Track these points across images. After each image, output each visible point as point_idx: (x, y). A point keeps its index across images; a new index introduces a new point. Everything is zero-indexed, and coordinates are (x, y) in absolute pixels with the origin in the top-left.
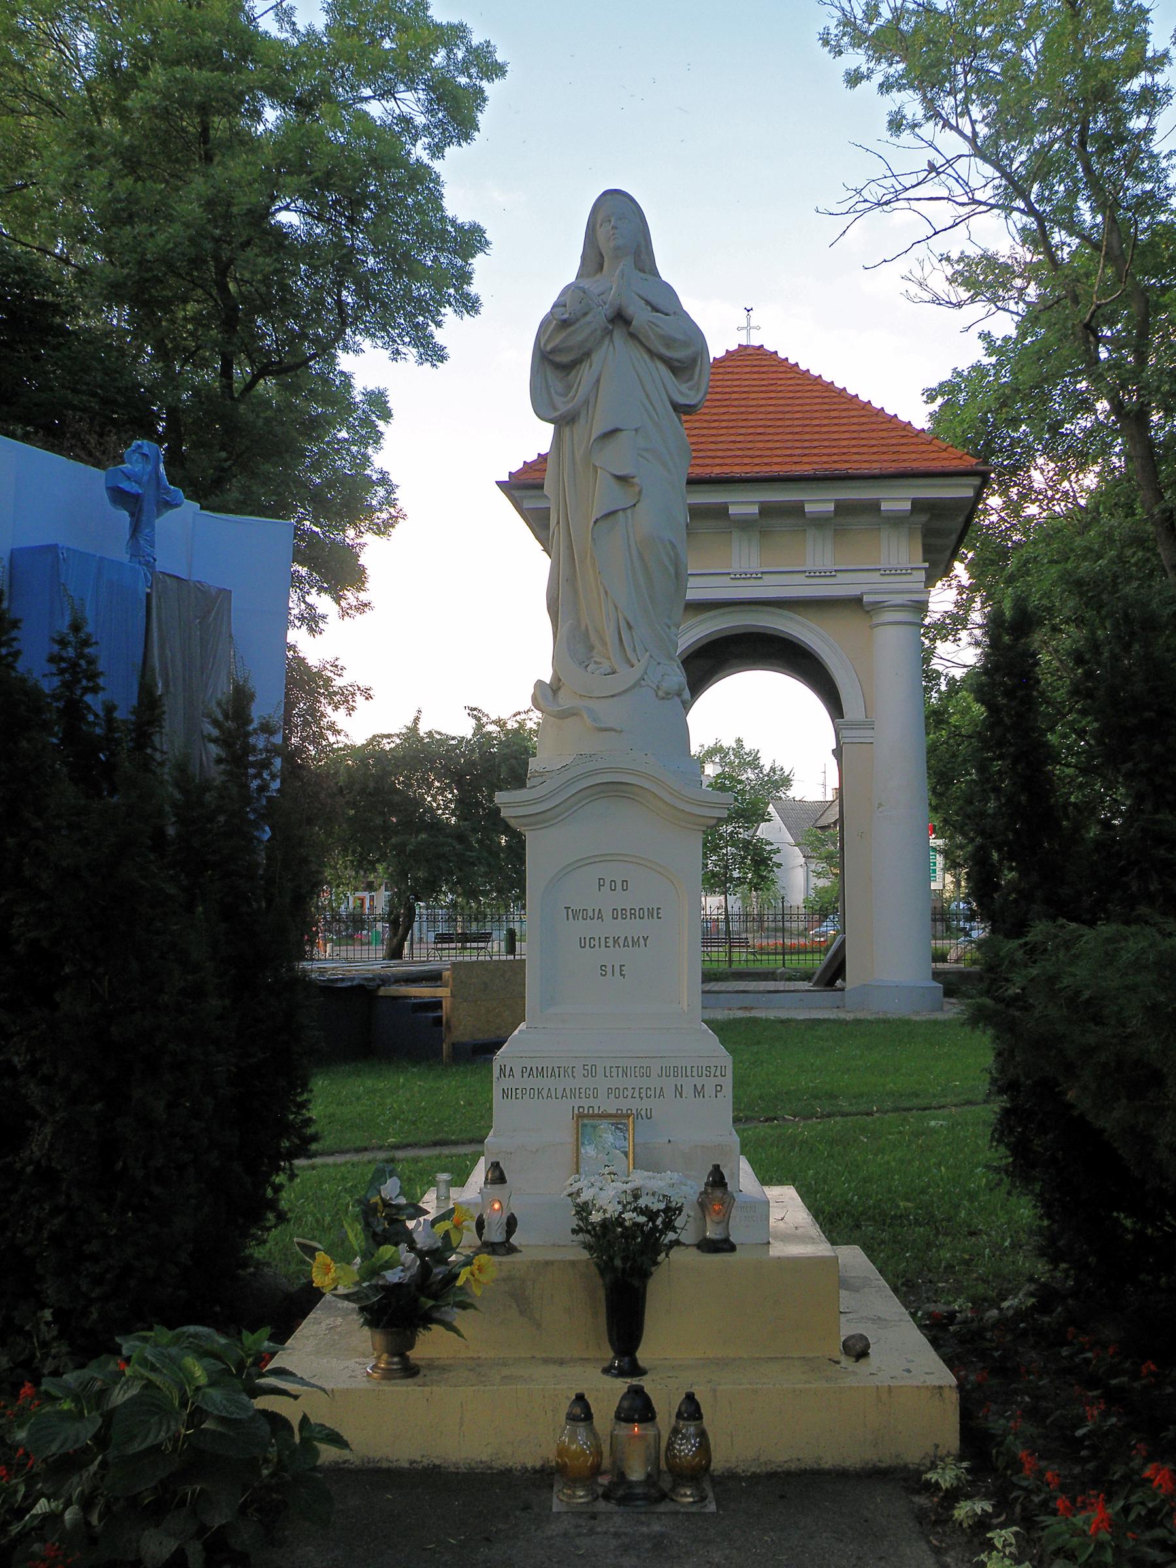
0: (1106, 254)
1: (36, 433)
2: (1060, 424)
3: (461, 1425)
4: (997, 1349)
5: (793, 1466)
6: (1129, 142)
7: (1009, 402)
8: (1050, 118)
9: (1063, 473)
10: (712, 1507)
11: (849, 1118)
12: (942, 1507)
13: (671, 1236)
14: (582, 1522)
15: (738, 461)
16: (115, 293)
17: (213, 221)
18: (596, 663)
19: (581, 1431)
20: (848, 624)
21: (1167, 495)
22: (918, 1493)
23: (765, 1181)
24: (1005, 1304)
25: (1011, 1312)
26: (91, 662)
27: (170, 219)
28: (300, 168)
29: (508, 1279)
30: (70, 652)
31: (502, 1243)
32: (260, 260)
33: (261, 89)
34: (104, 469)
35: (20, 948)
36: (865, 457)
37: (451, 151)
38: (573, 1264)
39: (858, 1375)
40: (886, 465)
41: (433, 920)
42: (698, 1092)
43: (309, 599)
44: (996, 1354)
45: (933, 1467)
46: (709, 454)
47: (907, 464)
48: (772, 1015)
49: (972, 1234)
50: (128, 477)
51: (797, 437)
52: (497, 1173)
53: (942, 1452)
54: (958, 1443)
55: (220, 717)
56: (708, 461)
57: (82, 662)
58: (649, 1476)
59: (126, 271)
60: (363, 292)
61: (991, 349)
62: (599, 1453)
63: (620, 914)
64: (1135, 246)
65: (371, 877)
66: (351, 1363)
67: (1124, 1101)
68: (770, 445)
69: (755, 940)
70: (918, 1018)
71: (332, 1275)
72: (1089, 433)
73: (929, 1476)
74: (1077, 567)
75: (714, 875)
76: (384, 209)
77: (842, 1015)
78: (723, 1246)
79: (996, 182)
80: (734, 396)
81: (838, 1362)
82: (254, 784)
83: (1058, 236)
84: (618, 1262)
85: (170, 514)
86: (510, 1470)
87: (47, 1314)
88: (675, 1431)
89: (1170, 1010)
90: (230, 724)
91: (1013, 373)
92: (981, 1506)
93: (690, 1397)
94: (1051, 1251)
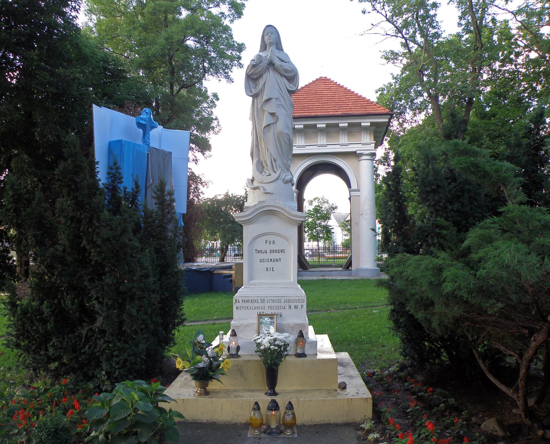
0: (425, 50)
1: (117, 107)
2: (414, 100)
3: (222, 409)
4: (386, 384)
5: (322, 423)
6: (430, 18)
7: (398, 93)
8: (408, 11)
9: (415, 115)
10: (296, 436)
11: (350, 310)
12: (365, 435)
13: (286, 353)
14: (256, 440)
15: (319, 111)
16: (140, 66)
17: (168, 44)
18: (265, 172)
19: (257, 412)
20: (354, 161)
21: (444, 121)
22: (359, 430)
23: (317, 332)
24: (390, 369)
25: (392, 372)
26: (120, 174)
27: (156, 44)
28: (193, 27)
29: (237, 366)
30: (114, 171)
31: (236, 354)
32: (181, 54)
33: (182, 6)
34: (135, 117)
35: (93, 263)
36: (357, 110)
37: (236, 21)
38: (256, 361)
39: (343, 395)
40: (363, 112)
41: (234, 250)
42: (296, 307)
43: (195, 154)
44: (386, 385)
45: (363, 423)
46: (311, 109)
47: (369, 112)
48: (330, 278)
49: (383, 346)
50: (142, 119)
51: (337, 104)
52: (234, 333)
53: (367, 418)
54: (371, 415)
55: (156, 190)
56: (311, 111)
57: (117, 174)
58: (277, 426)
59: (143, 60)
60: (210, 63)
61: (394, 78)
62: (262, 420)
63: (272, 251)
64: (433, 48)
65: (216, 237)
66: (190, 390)
67: (423, 311)
68: (329, 106)
69: (326, 255)
70: (372, 279)
71: (182, 365)
72: (422, 103)
73: (362, 426)
74: (419, 142)
75: (314, 236)
76: (216, 38)
77: (351, 278)
78: (303, 355)
79: (393, 29)
80: (318, 92)
81: (337, 391)
82: (167, 210)
83: (411, 44)
84: (269, 361)
85: (154, 130)
86: (236, 424)
87: (104, 373)
88: (285, 413)
89: (435, 283)
90: (159, 193)
91: (399, 85)
92: (376, 435)
93: (290, 403)
94: (404, 354)
